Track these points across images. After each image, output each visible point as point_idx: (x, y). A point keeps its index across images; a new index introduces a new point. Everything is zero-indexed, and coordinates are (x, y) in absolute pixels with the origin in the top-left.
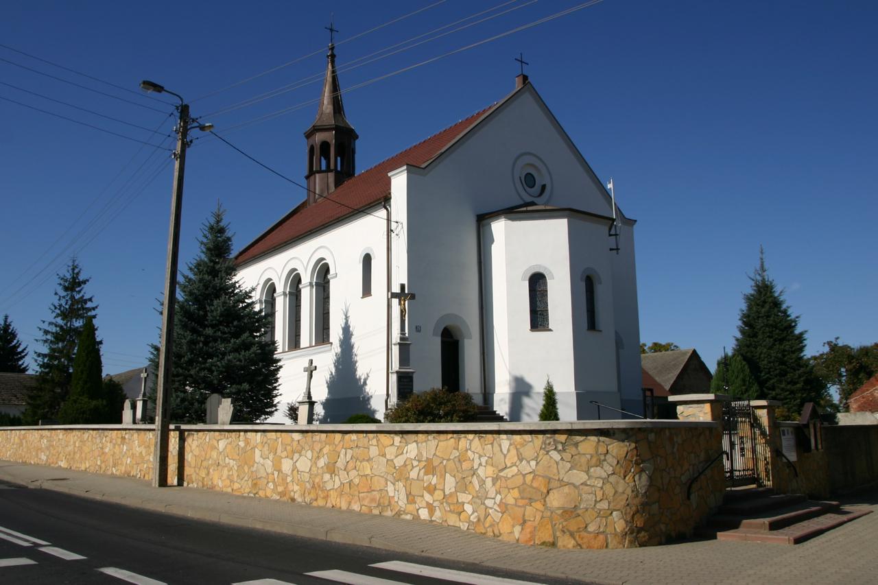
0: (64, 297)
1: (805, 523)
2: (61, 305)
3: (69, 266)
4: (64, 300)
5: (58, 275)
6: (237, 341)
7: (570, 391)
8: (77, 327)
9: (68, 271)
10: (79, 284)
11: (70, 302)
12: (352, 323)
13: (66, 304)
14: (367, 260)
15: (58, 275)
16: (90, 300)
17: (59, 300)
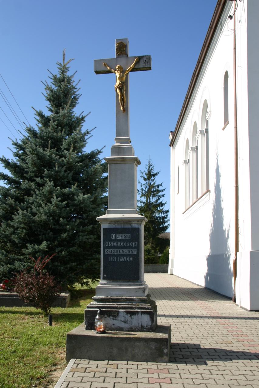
0: (144, 185)
1: (229, 79)
2: (142, 189)
3: (147, 165)
4: (144, 186)
5: (140, 171)
6: (81, 197)
7: (114, 58)
8: (153, 202)
9: (146, 168)
10: (154, 175)
11: (148, 187)
12: (219, 164)
13: (146, 189)
14: (227, 74)
15: (140, 171)
16: (161, 185)
17: (142, 186)
